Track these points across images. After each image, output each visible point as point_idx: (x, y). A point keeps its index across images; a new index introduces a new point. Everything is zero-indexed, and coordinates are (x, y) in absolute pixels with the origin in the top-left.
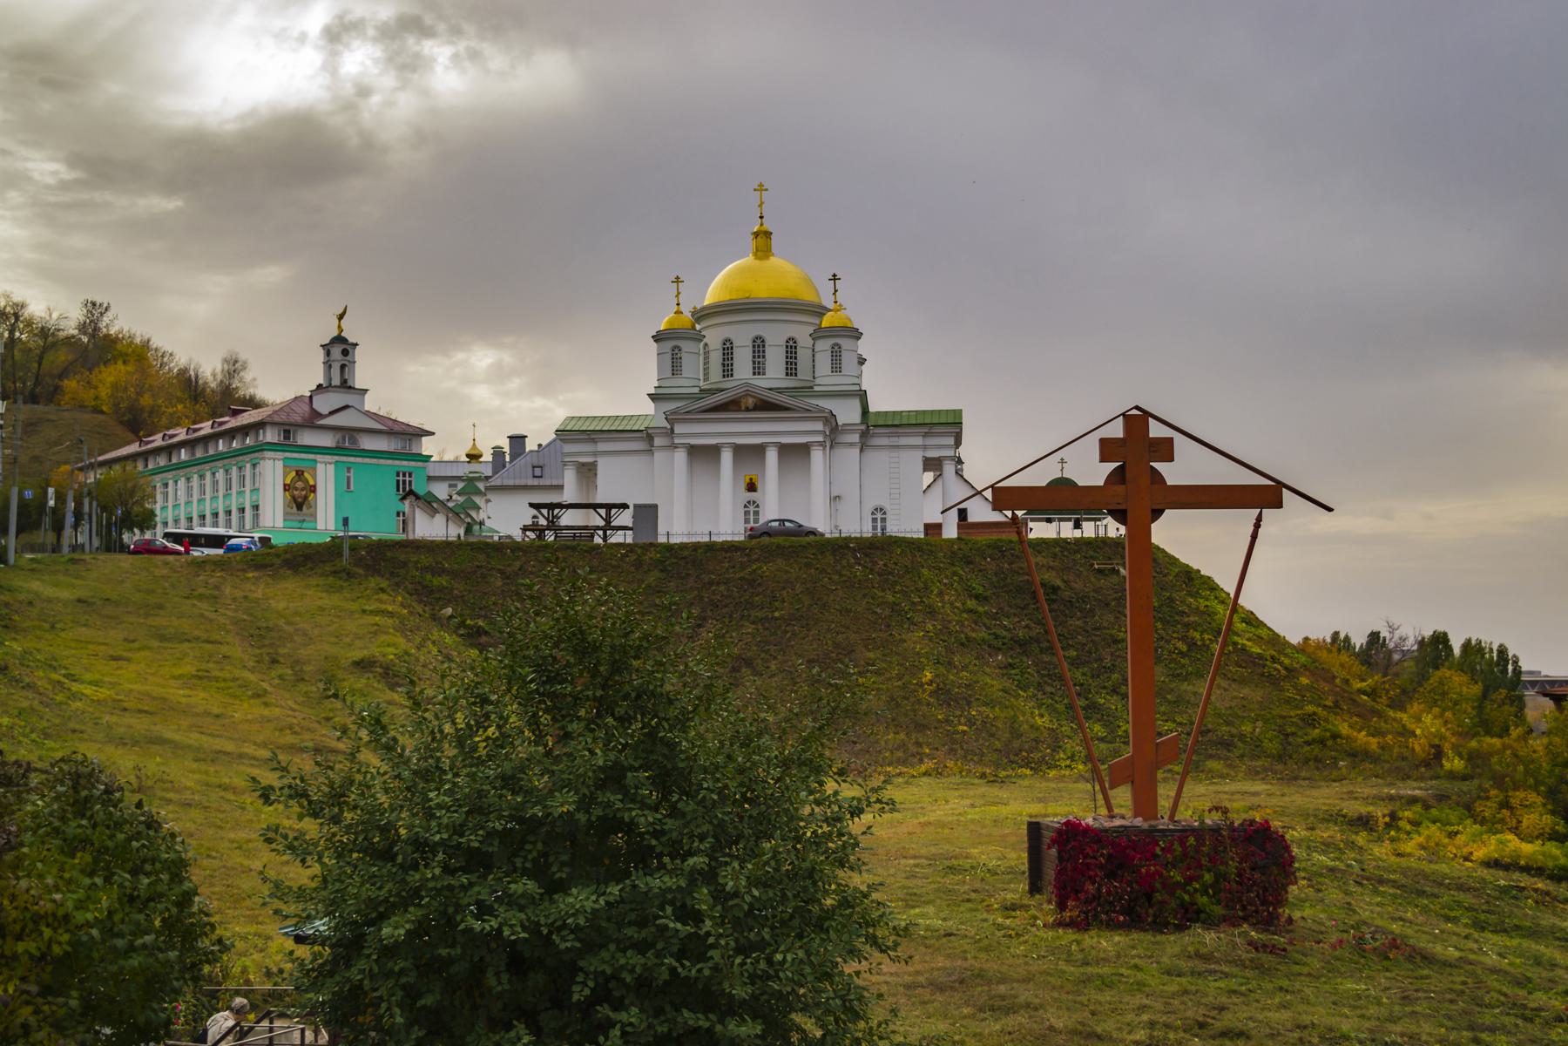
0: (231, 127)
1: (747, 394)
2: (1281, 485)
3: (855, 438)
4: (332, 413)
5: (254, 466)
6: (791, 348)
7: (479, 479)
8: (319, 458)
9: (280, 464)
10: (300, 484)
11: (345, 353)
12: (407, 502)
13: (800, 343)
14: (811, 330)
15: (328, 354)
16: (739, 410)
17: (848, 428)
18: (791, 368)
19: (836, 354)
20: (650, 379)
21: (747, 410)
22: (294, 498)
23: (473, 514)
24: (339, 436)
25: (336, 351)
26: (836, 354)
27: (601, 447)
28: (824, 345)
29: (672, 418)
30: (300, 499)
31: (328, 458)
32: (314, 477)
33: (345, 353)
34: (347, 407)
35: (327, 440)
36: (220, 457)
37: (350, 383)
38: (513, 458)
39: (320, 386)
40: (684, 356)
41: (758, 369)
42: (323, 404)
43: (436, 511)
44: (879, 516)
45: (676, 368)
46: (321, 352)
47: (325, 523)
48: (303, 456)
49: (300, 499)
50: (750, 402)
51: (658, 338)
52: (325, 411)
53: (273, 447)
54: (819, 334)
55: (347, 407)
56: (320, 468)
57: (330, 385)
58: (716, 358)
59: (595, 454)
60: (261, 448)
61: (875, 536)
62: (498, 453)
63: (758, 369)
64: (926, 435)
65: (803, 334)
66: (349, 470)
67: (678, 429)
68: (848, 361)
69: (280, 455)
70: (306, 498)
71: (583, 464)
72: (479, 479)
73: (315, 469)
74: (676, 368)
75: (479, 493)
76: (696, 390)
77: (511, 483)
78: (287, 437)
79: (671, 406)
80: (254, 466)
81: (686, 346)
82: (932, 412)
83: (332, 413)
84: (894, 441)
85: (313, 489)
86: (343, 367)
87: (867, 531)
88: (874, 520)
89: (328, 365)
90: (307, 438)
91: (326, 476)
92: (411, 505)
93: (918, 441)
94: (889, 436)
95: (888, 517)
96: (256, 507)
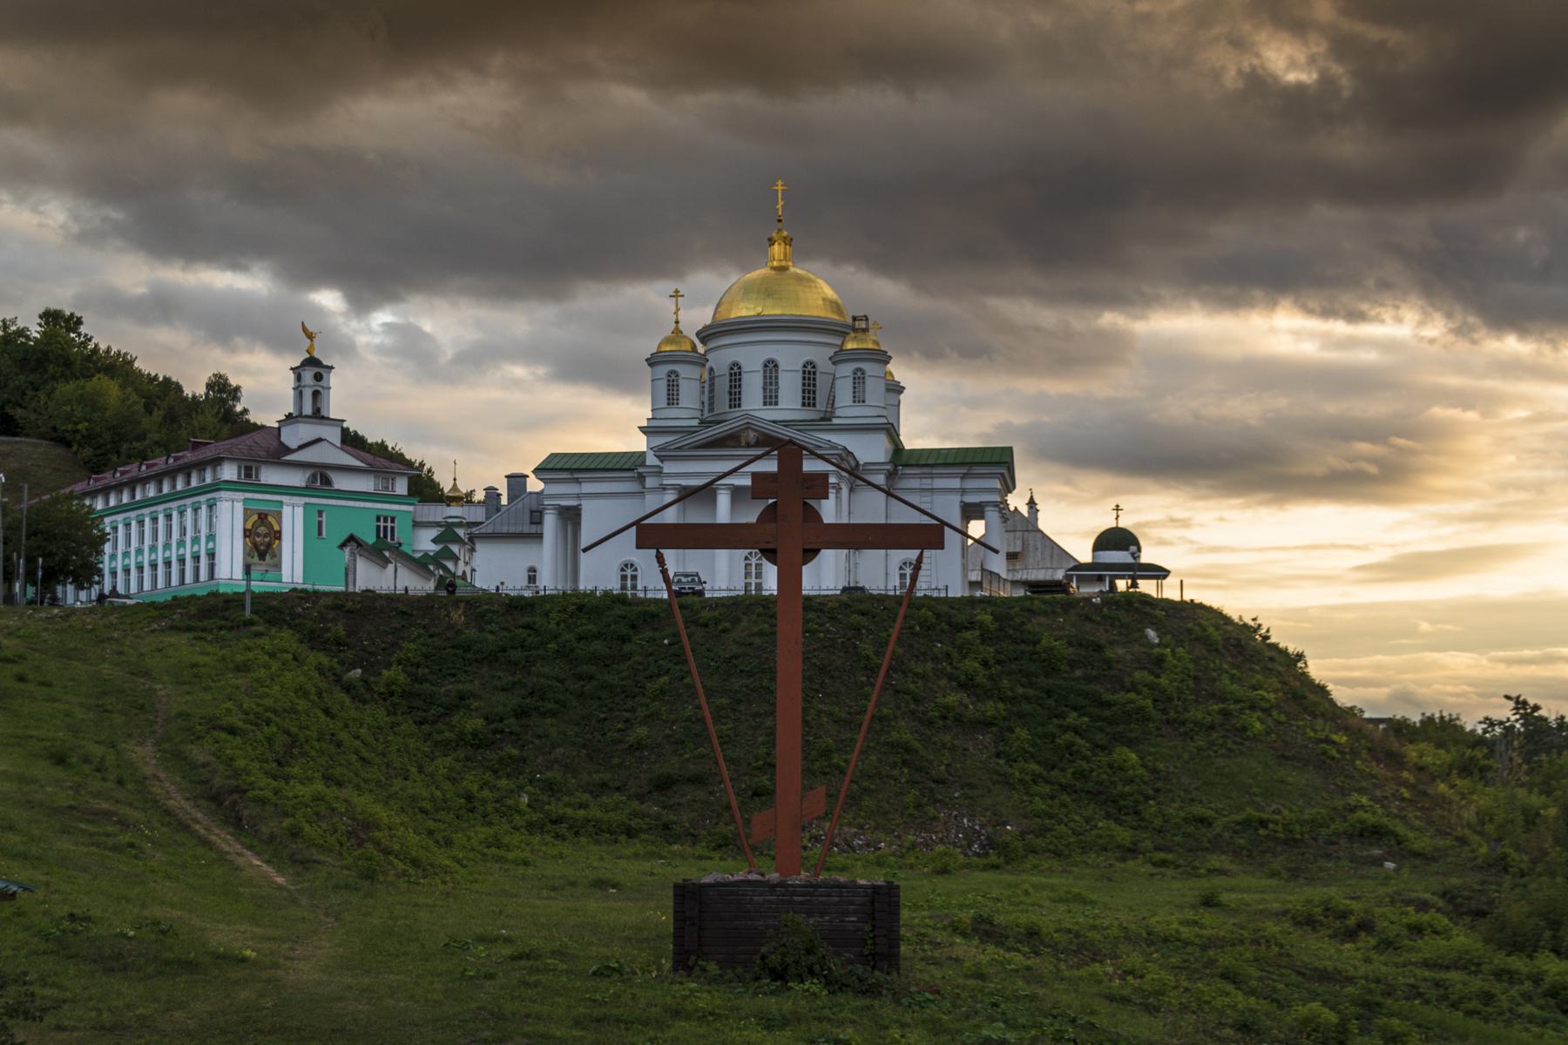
0: (1195, 304)
1: (748, 427)
2: (944, 523)
3: (880, 479)
4: (301, 447)
5: (210, 507)
6: (809, 373)
7: (460, 525)
8: (285, 499)
9: (239, 507)
10: (262, 530)
11: (318, 377)
12: (347, 550)
13: (820, 369)
14: (831, 352)
15: (299, 378)
16: (738, 446)
17: (873, 467)
18: (808, 399)
19: (859, 378)
20: (641, 411)
21: (748, 445)
22: (255, 545)
23: (450, 565)
24: (308, 473)
25: (308, 376)
26: (859, 378)
27: (587, 488)
28: (846, 369)
29: (663, 454)
30: (262, 542)
31: (296, 500)
32: (280, 523)
33: (318, 377)
34: (319, 440)
35: (297, 479)
36: (175, 496)
37: (323, 413)
38: (510, 499)
39: (289, 416)
40: (681, 382)
41: (771, 399)
42: (291, 437)
43: (387, 561)
44: (629, 572)
45: (672, 399)
46: (291, 376)
47: (292, 570)
48: (362, 504)
49: (262, 542)
50: (752, 435)
51: (653, 361)
52: (293, 445)
53: (230, 486)
54: (840, 357)
55: (319, 440)
56: (286, 511)
57: (300, 415)
58: (723, 385)
59: (578, 496)
60: (217, 486)
61: (747, 596)
62: (492, 493)
63: (771, 399)
64: (964, 477)
65: (821, 356)
66: (320, 513)
67: (669, 467)
68: (874, 391)
69: (241, 496)
70: (269, 545)
71: (568, 508)
72: (460, 525)
73: (279, 514)
74: (672, 399)
75: (458, 540)
76: (695, 422)
77: (505, 530)
78: (248, 476)
79: (660, 441)
80: (210, 507)
81: (685, 371)
82: (994, 449)
83: (301, 447)
84: (926, 483)
85: (278, 535)
86: (316, 394)
87: (614, 585)
88: (624, 578)
89: (299, 391)
90: (270, 476)
91: (293, 520)
92: (352, 554)
93: (955, 483)
94: (922, 476)
95: (639, 573)
96: (212, 555)
